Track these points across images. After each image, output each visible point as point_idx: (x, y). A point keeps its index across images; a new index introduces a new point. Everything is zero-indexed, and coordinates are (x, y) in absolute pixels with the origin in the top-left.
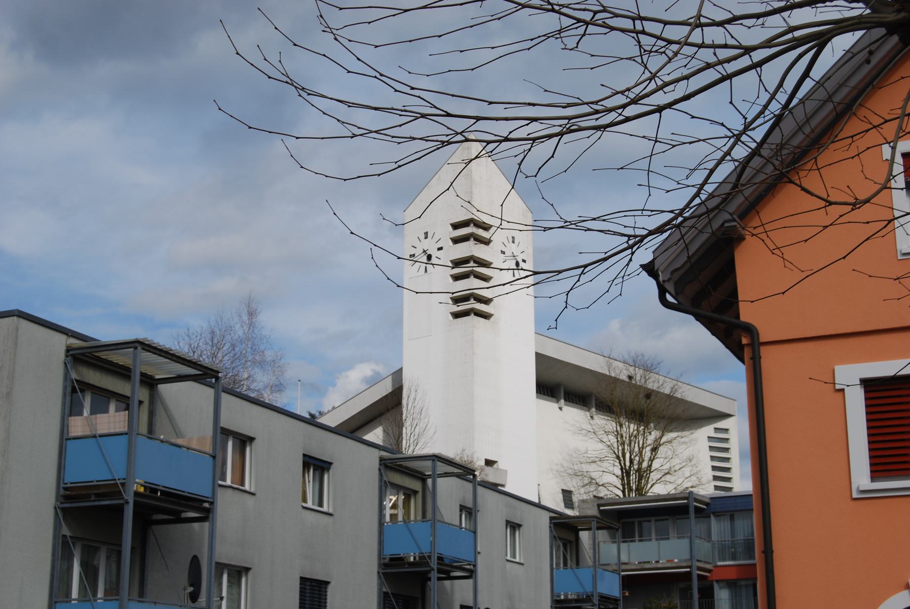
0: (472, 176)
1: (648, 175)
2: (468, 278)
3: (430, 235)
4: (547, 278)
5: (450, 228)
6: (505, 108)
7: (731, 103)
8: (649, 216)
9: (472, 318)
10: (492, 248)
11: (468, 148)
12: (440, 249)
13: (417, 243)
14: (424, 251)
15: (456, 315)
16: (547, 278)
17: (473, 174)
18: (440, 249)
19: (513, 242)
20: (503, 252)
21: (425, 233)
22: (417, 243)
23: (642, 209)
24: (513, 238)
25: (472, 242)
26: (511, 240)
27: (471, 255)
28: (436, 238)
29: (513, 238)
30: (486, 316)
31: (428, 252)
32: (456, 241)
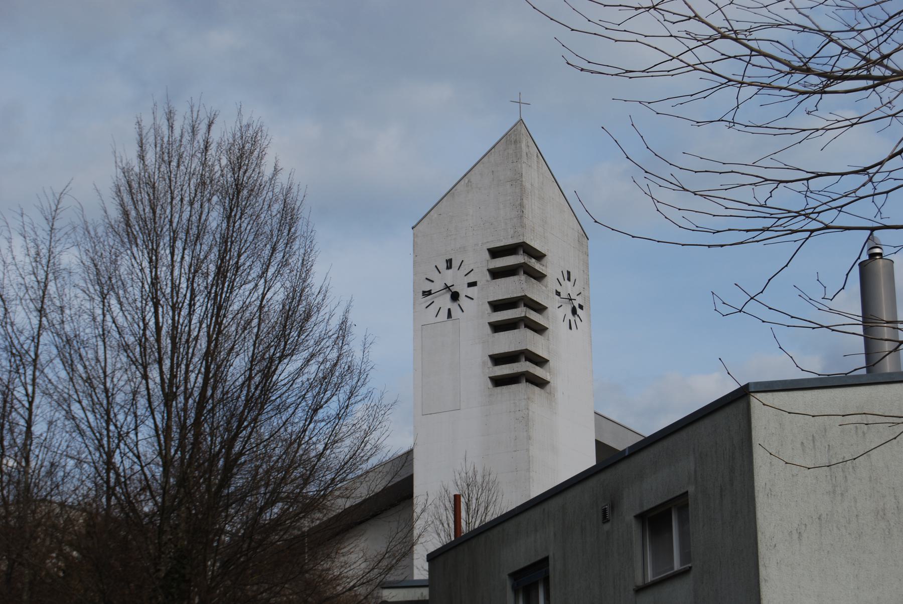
0: (522, 181)
1: (754, 65)
2: (515, 328)
3: (455, 264)
4: (765, 217)
5: (487, 255)
6: (800, 296)
7: (771, 196)
8: (814, 328)
9: (522, 388)
10: (546, 287)
11: (515, 142)
12: (472, 284)
13: (434, 275)
14: (447, 287)
15: (498, 382)
16: (765, 217)
17: (524, 179)
18: (472, 284)
19: (569, 279)
20: (558, 294)
21: (447, 261)
22: (434, 275)
23: (728, 19)
24: (569, 273)
25: (522, 277)
26: (566, 276)
27: (523, 294)
28: (465, 269)
29: (569, 273)
30: (541, 383)
31: (453, 289)
32: (496, 274)
